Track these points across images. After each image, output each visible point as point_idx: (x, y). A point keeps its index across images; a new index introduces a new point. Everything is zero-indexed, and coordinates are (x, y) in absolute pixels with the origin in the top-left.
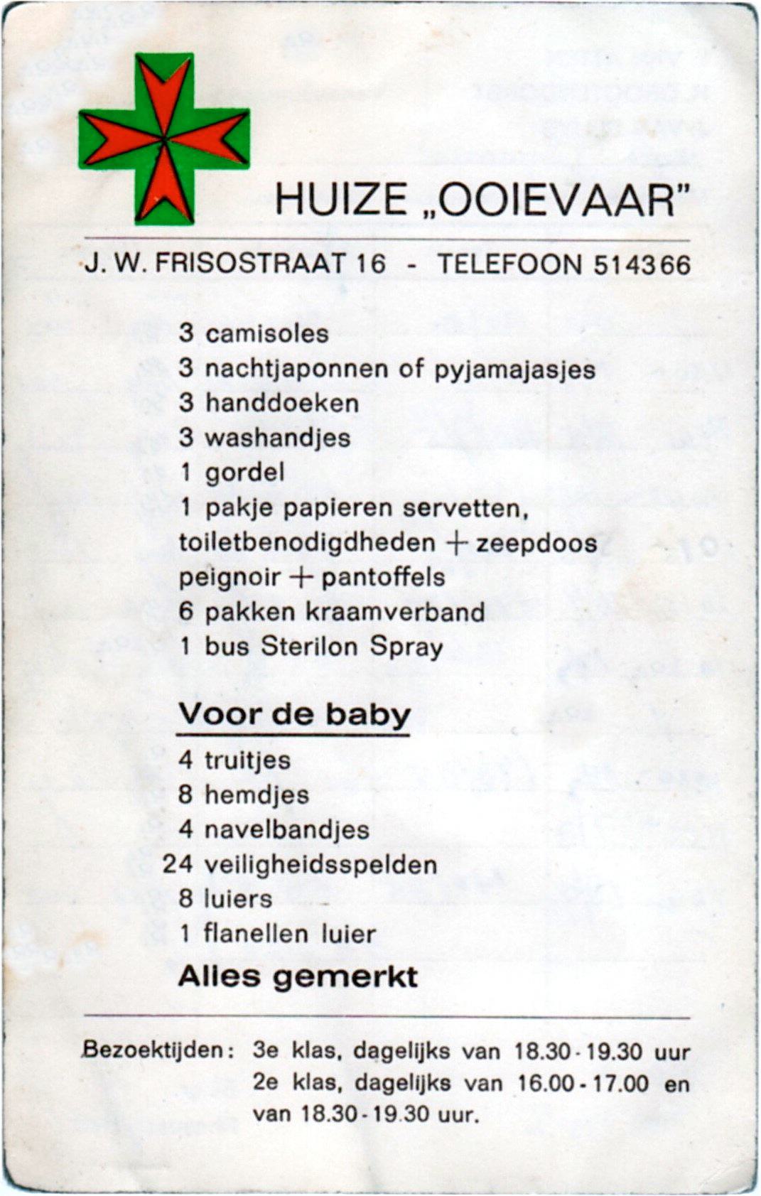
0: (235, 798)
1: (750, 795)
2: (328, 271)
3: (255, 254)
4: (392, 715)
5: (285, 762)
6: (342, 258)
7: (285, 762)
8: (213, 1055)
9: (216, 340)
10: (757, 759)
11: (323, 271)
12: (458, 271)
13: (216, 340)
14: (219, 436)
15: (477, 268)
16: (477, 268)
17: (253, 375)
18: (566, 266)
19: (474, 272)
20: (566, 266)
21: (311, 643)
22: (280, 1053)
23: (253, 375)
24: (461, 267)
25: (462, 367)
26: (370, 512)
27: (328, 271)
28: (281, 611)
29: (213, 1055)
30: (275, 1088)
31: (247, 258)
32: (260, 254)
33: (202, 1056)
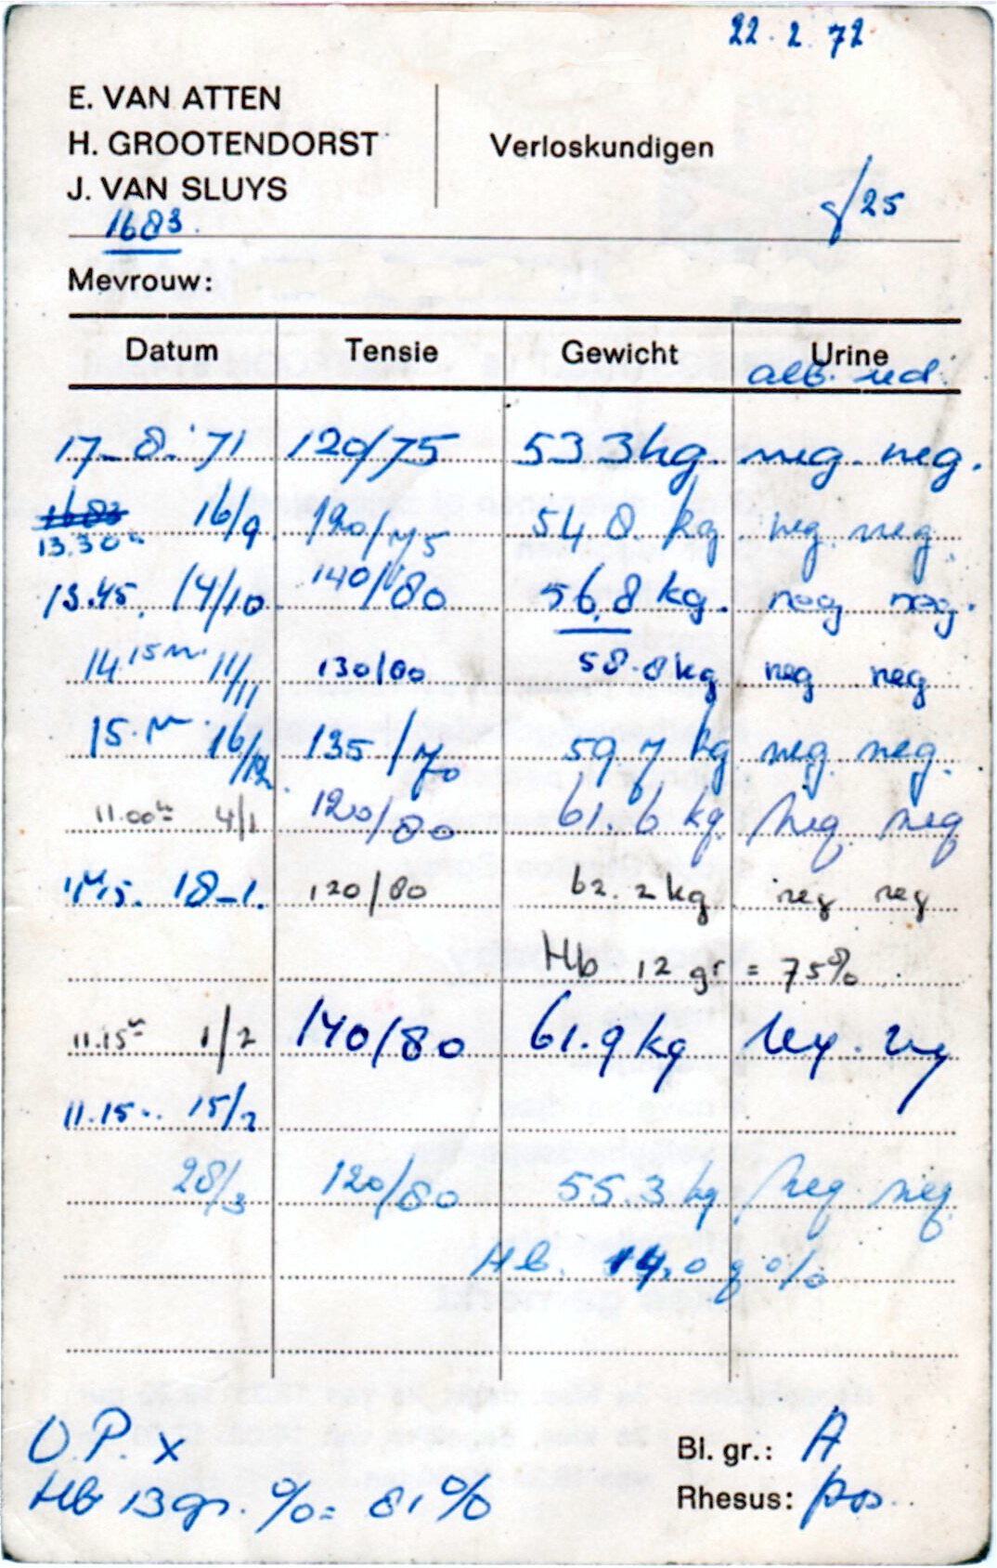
0: (379, 356)
1: (806, 307)
2: (201, 107)
3: (358, 133)
4: (603, 354)
5: (431, 354)
6: (374, 138)
7: (431, 354)
8: (384, 358)
9: (646, 361)
10: (5, 491)
11: (197, 107)
12: (229, 152)
13: (646, 361)
14: (619, 351)
15: (212, 194)
16: (212, 194)
17: (654, 361)
18: (262, 140)
19: (208, 198)
20: (262, 140)
21: (843, 352)
22: (440, 356)
23: (654, 361)
24: (249, 102)
25: (623, 351)
26: (371, 356)
27: (201, 107)
28: (380, 350)
29: (384, 358)
30: (434, 360)
31: (349, 138)
32: (363, 134)
33: (427, 360)
